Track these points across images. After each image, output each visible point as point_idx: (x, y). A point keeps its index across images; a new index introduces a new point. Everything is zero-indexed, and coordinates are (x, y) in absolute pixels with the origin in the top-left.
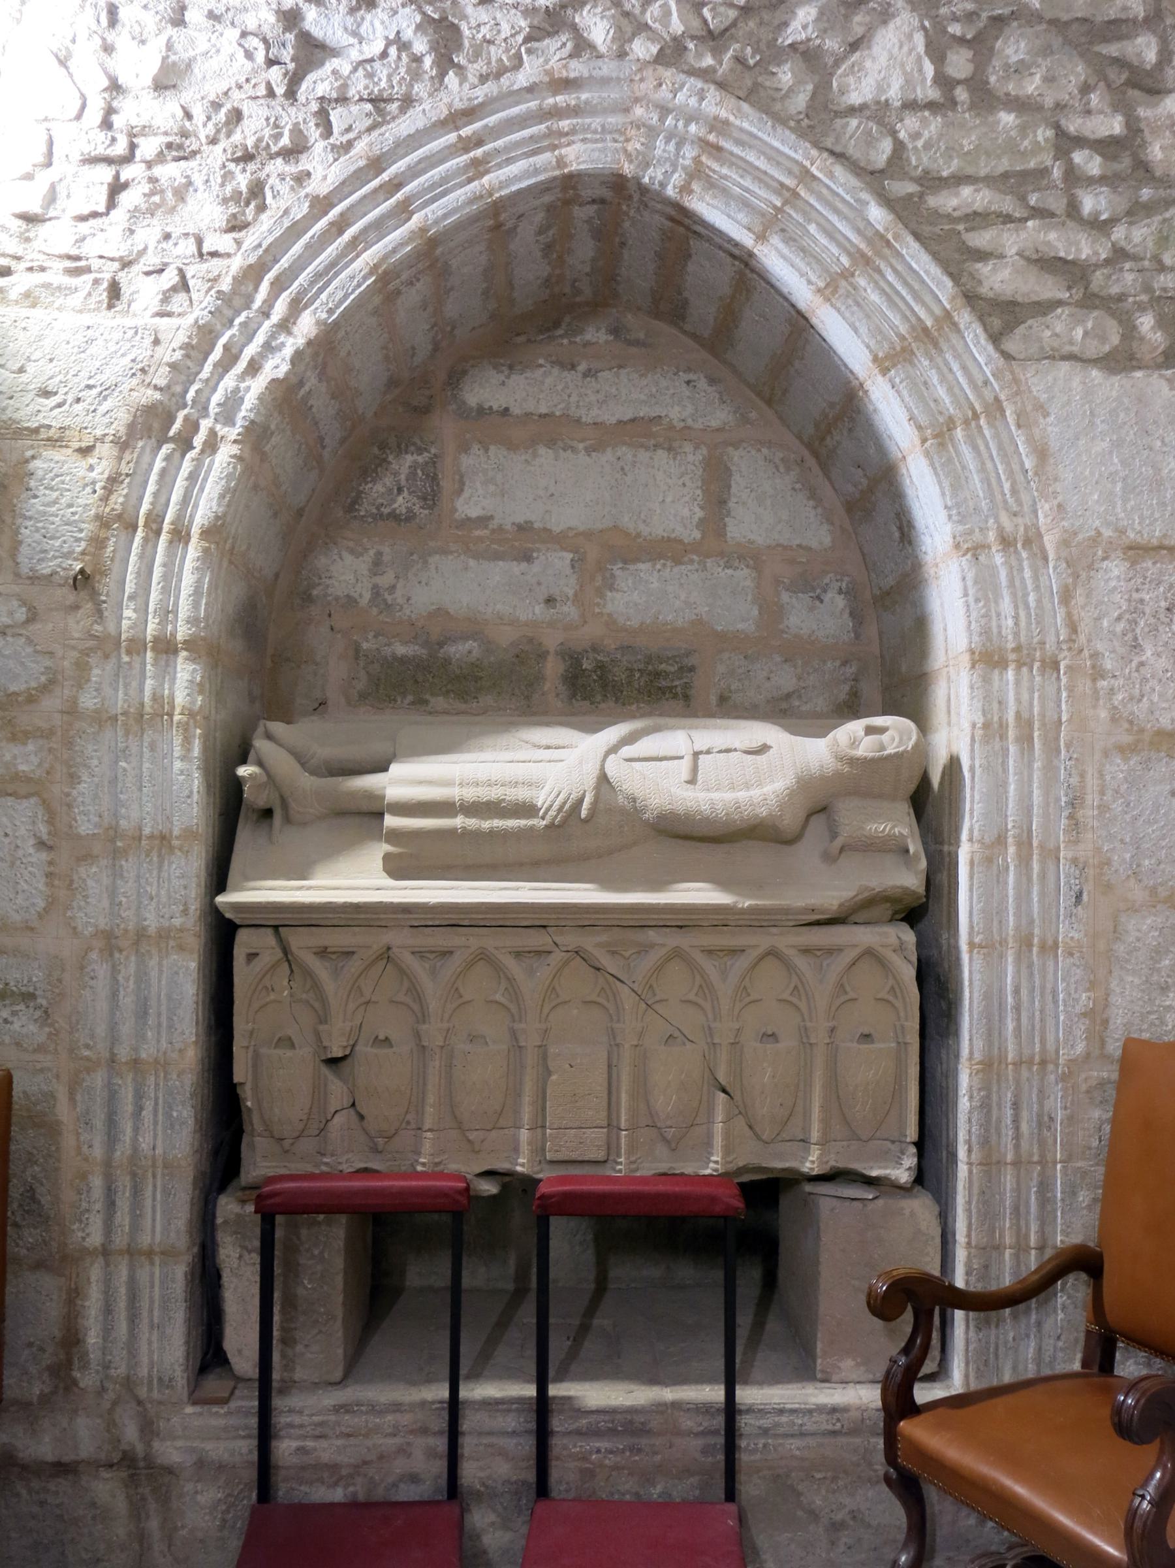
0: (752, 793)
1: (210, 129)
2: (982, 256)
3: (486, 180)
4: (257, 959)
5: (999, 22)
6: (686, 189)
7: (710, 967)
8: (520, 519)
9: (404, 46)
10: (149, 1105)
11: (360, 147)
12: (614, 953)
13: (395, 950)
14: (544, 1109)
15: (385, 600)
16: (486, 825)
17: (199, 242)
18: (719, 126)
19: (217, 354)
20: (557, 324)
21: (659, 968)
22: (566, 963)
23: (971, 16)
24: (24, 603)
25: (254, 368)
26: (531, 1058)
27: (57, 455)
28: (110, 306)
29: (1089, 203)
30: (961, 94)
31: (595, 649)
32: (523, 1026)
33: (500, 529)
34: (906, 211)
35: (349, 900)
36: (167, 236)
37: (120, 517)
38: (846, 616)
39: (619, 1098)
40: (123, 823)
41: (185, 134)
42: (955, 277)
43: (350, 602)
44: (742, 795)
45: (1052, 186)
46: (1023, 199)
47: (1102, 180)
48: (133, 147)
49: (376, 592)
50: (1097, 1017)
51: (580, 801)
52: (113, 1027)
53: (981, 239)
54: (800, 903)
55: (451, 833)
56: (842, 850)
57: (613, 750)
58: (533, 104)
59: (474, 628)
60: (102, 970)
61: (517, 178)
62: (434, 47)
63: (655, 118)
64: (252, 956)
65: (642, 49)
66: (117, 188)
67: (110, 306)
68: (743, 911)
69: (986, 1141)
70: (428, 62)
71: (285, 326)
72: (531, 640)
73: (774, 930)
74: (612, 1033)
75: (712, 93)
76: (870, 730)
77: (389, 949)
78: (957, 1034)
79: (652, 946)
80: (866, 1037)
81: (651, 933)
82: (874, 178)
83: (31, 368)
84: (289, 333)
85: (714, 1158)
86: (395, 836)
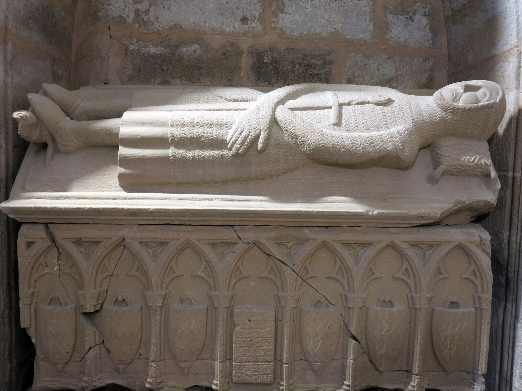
0: (381, 133)
7: (347, 255)
12: (280, 244)
13: (127, 241)
14: (231, 348)
15: (143, 19)
16: (190, 154)
21: (312, 255)
22: (247, 251)
31: (272, 49)
32: (217, 293)
35: (93, 206)
38: (427, 30)
39: (282, 342)
43: (122, 20)
49: (137, 14)
51: (257, 137)
54: (413, 212)
55: (165, 160)
56: (443, 174)
57: (282, 102)
59: (197, 36)
64: (29, 244)
68: (373, 217)
72: (232, 44)
73: (393, 230)
74: (278, 299)
76: (468, 89)
77: (124, 240)
79: (307, 240)
81: (306, 231)
85: (346, 383)
86: (126, 162)
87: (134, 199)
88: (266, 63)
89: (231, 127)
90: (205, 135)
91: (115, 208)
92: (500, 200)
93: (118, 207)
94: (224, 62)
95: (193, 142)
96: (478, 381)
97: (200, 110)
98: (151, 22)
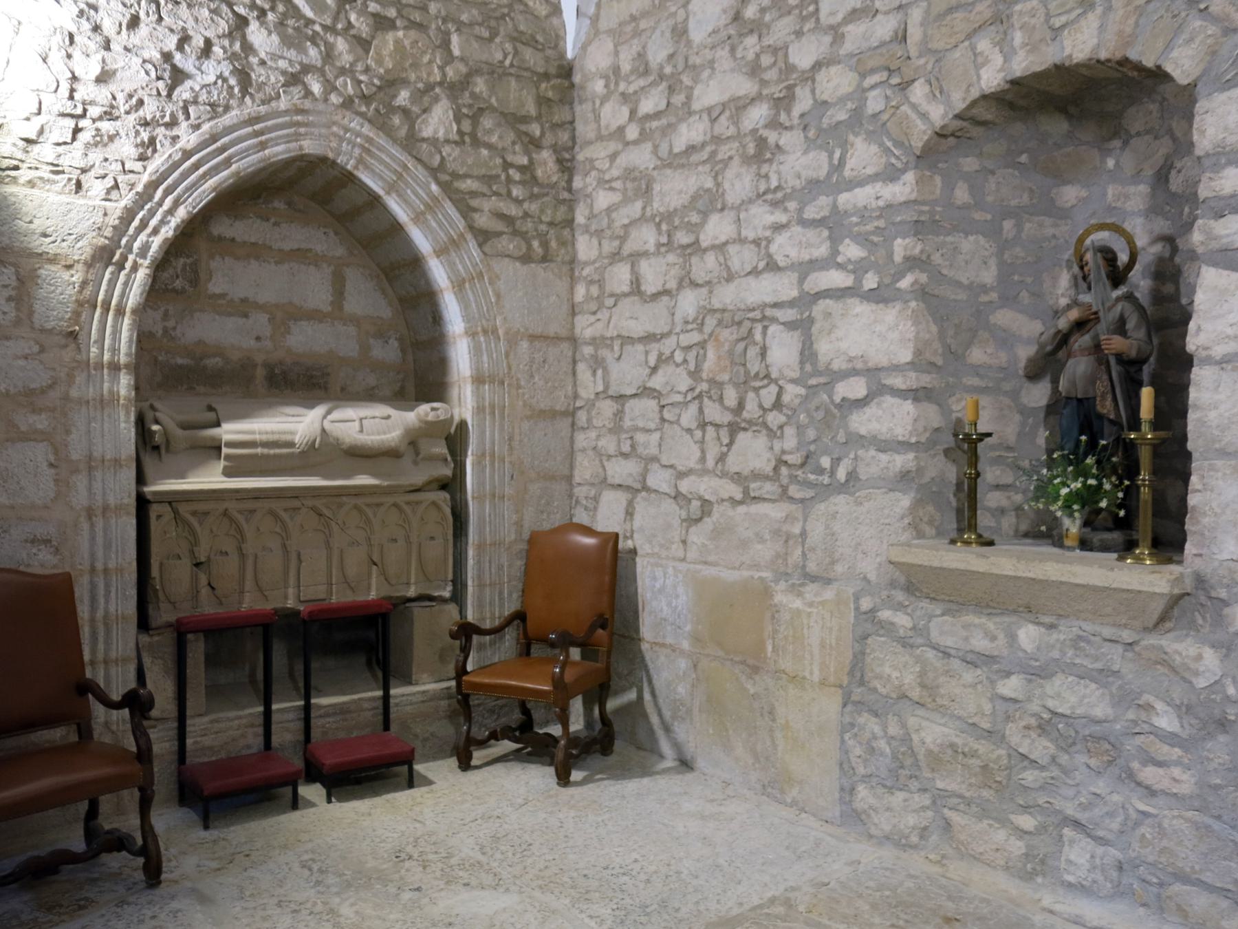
1: (127, 107)
2: (475, 210)
3: (266, 152)
5: (481, 110)
6: (356, 167)
8: (242, 296)
9: (225, 80)
10: (113, 590)
11: (206, 127)
16: (272, 452)
17: (123, 165)
18: (369, 140)
19: (136, 223)
20: (259, 197)
23: (470, 106)
24: (37, 343)
25: (155, 231)
26: (294, 556)
27: (53, 268)
28: (77, 192)
29: (515, 192)
30: (467, 139)
33: (232, 300)
34: (446, 187)
36: (106, 160)
37: (88, 302)
40: (95, 454)
41: (112, 107)
42: (465, 218)
44: (383, 437)
45: (500, 183)
46: (490, 187)
47: (520, 182)
48: (85, 111)
49: (165, 330)
50: (519, 524)
51: (315, 441)
52: (93, 555)
53: (474, 203)
55: (256, 455)
58: (287, 119)
60: (85, 526)
61: (282, 153)
62: (239, 83)
63: (342, 133)
64: (159, 517)
65: (335, 99)
66: (77, 131)
67: (77, 192)
69: (480, 577)
70: (236, 90)
71: (171, 212)
75: (366, 125)
76: (433, 409)
78: (466, 535)
80: (432, 538)
81: (344, 498)
82: (434, 172)
83: (36, 221)
84: (172, 215)
92: (454, 475)
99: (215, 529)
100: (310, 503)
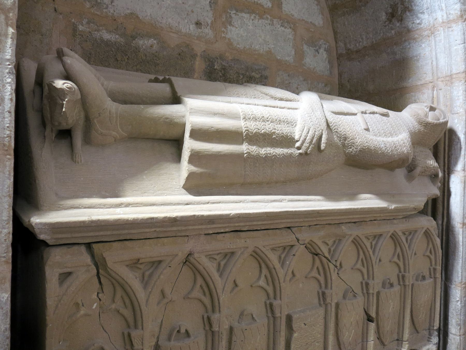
4: (70, 279)
13: (196, 255)
16: (263, 151)
38: (327, 62)
51: (320, 137)
55: (238, 157)
59: (154, 31)
64: (65, 276)
72: (188, 46)
87: (208, 203)
88: (216, 69)
89: (296, 125)
90: (277, 132)
91: (194, 216)
93: (197, 213)
94: (180, 62)
95: (265, 139)
96: (434, 335)
97: (258, 105)
98: (105, 4)
99: (168, 291)
100: (305, 236)
